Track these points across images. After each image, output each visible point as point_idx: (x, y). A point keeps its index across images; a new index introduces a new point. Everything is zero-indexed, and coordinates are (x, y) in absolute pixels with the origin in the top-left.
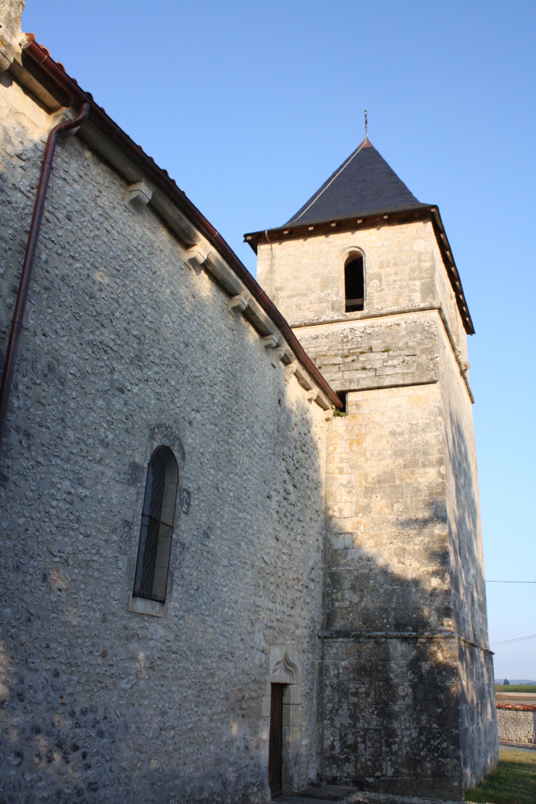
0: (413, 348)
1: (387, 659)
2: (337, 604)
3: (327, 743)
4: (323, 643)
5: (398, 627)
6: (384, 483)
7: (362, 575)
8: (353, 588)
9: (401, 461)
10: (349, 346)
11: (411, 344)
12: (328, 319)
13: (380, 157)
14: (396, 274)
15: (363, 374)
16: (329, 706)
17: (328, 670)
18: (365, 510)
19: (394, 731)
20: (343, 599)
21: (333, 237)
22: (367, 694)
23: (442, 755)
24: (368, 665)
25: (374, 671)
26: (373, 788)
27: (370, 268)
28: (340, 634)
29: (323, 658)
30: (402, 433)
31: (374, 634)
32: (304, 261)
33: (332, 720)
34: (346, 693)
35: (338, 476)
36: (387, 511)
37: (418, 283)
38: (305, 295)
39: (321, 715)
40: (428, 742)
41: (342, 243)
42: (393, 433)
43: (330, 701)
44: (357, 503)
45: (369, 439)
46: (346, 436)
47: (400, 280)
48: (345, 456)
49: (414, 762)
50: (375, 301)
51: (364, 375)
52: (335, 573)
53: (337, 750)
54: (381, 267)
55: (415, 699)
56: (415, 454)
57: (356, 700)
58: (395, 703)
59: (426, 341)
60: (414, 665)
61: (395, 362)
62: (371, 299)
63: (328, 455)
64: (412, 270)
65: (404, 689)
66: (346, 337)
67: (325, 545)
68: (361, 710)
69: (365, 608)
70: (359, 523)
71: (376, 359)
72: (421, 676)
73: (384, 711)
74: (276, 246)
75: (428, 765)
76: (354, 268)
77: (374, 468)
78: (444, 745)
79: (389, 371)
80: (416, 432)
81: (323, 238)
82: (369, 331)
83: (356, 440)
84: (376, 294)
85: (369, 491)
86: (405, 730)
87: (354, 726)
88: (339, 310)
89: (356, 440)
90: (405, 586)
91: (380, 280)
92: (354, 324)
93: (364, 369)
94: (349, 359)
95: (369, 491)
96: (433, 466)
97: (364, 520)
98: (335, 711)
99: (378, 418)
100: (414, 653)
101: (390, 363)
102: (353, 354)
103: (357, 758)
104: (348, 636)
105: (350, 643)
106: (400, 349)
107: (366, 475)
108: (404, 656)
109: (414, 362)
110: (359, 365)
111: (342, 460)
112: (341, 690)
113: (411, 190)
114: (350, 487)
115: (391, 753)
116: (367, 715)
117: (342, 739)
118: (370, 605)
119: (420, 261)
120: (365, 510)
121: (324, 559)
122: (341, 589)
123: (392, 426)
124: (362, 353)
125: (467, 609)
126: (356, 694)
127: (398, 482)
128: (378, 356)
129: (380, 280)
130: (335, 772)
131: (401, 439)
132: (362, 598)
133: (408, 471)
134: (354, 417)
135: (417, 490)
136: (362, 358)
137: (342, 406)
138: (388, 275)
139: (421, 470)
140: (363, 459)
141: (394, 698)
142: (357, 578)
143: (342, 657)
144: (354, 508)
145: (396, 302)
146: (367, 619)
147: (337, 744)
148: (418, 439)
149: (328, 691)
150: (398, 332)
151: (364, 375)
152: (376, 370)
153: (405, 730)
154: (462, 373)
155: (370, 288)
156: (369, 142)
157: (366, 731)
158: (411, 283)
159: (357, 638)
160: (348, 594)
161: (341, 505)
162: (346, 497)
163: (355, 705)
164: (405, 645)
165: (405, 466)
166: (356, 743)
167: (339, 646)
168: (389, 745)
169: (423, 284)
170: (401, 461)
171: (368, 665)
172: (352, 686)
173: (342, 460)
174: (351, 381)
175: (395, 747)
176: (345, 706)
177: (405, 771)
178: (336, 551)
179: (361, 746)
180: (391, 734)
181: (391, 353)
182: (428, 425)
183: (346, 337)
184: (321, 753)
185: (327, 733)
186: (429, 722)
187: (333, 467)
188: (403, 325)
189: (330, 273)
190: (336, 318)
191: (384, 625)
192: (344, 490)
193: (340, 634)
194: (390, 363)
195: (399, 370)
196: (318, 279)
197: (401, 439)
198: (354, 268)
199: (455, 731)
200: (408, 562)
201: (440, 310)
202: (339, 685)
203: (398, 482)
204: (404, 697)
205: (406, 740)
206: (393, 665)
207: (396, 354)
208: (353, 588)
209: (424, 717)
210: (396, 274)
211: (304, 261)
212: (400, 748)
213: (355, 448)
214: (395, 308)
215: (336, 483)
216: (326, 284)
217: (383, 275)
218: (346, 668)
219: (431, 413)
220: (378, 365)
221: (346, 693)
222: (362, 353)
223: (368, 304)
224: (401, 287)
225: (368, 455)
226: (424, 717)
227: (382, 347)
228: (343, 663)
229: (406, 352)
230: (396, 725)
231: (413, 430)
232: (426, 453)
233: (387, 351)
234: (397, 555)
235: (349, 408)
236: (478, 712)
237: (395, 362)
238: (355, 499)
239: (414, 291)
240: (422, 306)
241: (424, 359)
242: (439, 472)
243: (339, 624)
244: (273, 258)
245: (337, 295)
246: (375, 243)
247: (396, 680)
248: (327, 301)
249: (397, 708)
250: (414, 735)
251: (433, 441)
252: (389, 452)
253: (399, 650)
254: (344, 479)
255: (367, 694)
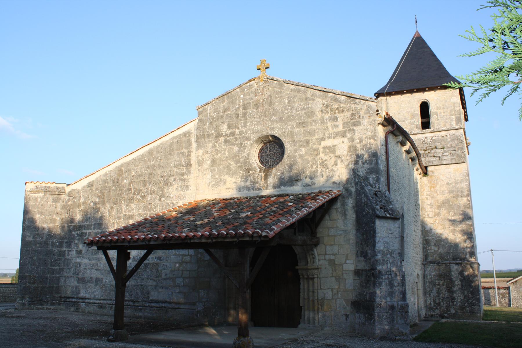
0: (454, 147)
1: (450, 271)
2: (429, 251)
3: (428, 303)
4: (425, 266)
5: (454, 259)
6: (445, 203)
7: (438, 240)
8: (435, 245)
9: (452, 195)
10: (426, 145)
11: (453, 145)
12: (415, 133)
13: (425, 43)
14: (444, 112)
15: (433, 159)
16: (428, 289)
17: (427, 276)
18: (438, 214)
19: (454, 297)
20: (431, 249)
21: (415, 95)
22: (443, 285)
23: (473, 305)
24: (443, 274)
25: (446, 276)
26: (447, 318)
27: (432, 109)
28: (431, 262)
29: (425, 272)
30: (452, 184)
31: (445, 262)
32: (402, 106)
33: (430, 295)
34: (435, 285)
35: (426, 201)
36: (447, 215)
37: (454, 117)
38: (404, 121)
39: (425, 293)
40: (468, 301)
41: (419, 97)
42: (448, 184)
43: (429, 287)
44: (435, 212)
45: (438, 186)
46: (429, 185)
47: (446, 116)
48: (428, 193)
49: (462, 308)
50: (436, 125)
51: (434, 159)
52: (427, 239)
53: (432, 305)
54: (437, 109)
55: (462, 285)
56: (457, 192)
57: (439, 287)
58: (454, 287)
59: (459, 144)
60: (461, 273)
61: (447, 154)
62: (434, 124)
63: (421, 192)
64: (451, 111)
65: (457, 282)
66: (424, 141)
67: (422, 228)
68: (441, 290)
69: (440, 252)
70: (436, 220)
71: (439, 152)
72: (464, 277)
73: (450, 290)
74: (388, 98)
75: (468, 309)
76: (424, 107)
77: (441, 198)
78: (474, 302)
79: (445, 158)
80: (458, 183)
81: (410, 94)
82: (434, 138)
83: (433, 186)
84: (435, 122)
85: (439, 207)
86: (459, 297)
87: (439, 296)
88: (419, 129)
89: (433, 186)
90: (456, 245)
91: (437, 115)
92: (427, 135)
93: (434, 156)
94: (427, 152)
95: (439, 207)
96: (465, 197)
97: (438, 219)
98: (431, 291)
99: (441, 177)
100: (461, 269)
101: (445, 154)
102: (428, 149)
103: (440, 307)
104: (434, 263)
105: (435, 266)
106: (449, 148)
107: (438, 201)
108: (457, 270)
109: (455, 154)
110: (431, 155)
111: (427, 195)
112: (433, 283)
113: (445, 66)
114: (431, 206)
115: (453, 305)
116: (444, 292)
117: (434, 301)
118: (442, 251)
119: (454, 107)
120: (438, 214)
121: (422, 234)
122: (430, 245)
123: (447, 181)
124: (432, 149)
125: (253, 159)
126: (439, 285)
127: (451, 203)
128: (440, 151)
129: (437, 115)
130: (432, 313)
131: (451, 186)
132: (439, 249)
133: (455, 199)
134: (431, 177)
135: (459, 207)
136: (433, 151)
137: (425, 171)
138: (440, 113)
139: (461, 199)
140: (436, 194)
141: (454, 286)
142: (436, 241)
143: (433, 271)
144: (434, 214)
145: (445, 126)
146: (441, 256)
147: (432, 303)
148: (458, 186)
149: (427, 284)
150: (447, 139)
151: (434, 159)
152: (439, 157)
153: (459, 297)
154: (467, 147)
155: (433, 119)
156: (418, 33)
157: (443, 298)
158: (451, 117)
159: (438, 264)
160: (433, 247)
161: (428, 213)
162: (430, 210)
163: (439, 289)
164: (457, 266)
165: (454, 197)
166: (440, 302)
167: (431, 267)
168: (452, 302)
169: (456, 117)
170: (452, 195)
171: (443, 274)
172: (437, 282)
173: (427, 195)
174: (429, 162)
175: (455, 303)
176: (435, 289)
177: (459, 311)
178: (427, 231)
179: (442, 303)
180: (453, 298)
181: (445, 149)
182: (462, 180)
183: (424, 141)
184: (426, 306)
185: (428, 299)
186: (468, 294)
187: (424, 197)
188: (449, 136)
189: (414, 111)
190: (419, 132)
191: (448, 259)
192: (429, 207)
193: (431, 262)
194: (445, 154)
195: (449, 157)
196: (409, 114)
197: (451, 186)
198: (424, 107)
199: (478, 297)
200: (457, 235)
201: (464, 129)
202: (432, 282)
203: (451, 203)
204: (457, 285)
205: (459, 300)
206: (453, 274)
207: (447, 150)
208: (435, 245)
209: (466, 292)
210: (444, 112)
211: (402, 106)
212: (457, 303)
213: (432, 189)
214: (444, 128)
215: (425, 204)
216: (413, 116)
217: (438, 113)
218: (434, 275)
219: (464, 175)
220: (440, 155)
221: (435, 285)
222: (432, 149)
223: (433, 126)
224: (446, 119)
225: (438, 192)
226: (466, 292)
227: (441, 146)
228: (433, 273)
229: (451, 149)
230: (455, 295)
231: (456, 182)
232: (462, 192)
233: (443, 148)
234: (452, 232)
235: (429, 173)
236: (304, 299)
237: (447, 154)
238: (434, 210)
239: (453, 120)
240: (456, 127)
241: (459, 152)
242: (468, 200)
243: (430, 259)
244: (387, 103)
245: (418, 122)
246: (432, 97)
247: (455, 279)
248: (414, 124)
249: (455, 289)
250: (462, 298)
251: (465, 187)
252: (447, 191)
253: (455, 268)
254: (429, 202)
255: (443, 285)
